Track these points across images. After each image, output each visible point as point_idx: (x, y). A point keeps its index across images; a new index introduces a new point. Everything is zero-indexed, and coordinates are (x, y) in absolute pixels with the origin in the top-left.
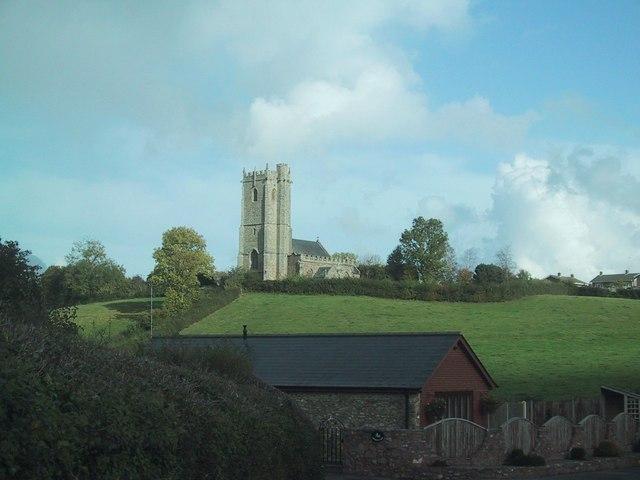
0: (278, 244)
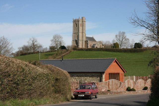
0: (82, 38)
